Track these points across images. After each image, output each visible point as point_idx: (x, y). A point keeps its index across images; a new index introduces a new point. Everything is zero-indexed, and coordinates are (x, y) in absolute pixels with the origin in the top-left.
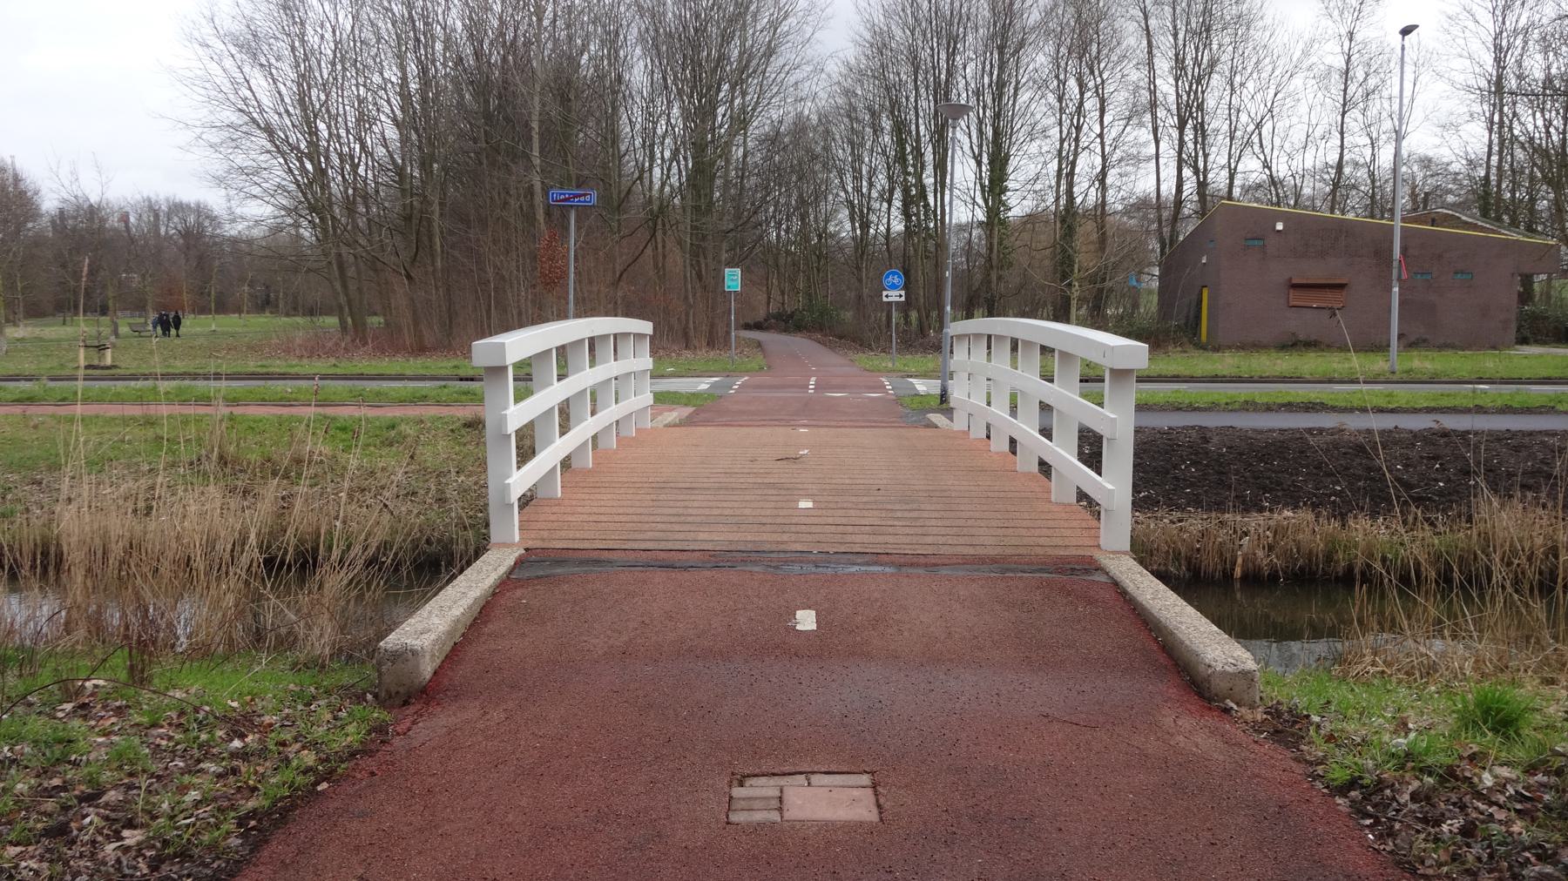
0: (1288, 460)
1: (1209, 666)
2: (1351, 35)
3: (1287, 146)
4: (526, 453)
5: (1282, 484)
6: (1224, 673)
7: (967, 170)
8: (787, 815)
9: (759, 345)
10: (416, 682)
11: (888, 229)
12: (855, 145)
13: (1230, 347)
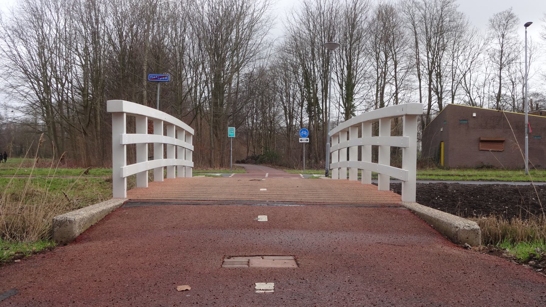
0: (484, 196)
1: (457, 227)
2: (503, 36)
3: (476, 84)
4: (132, 159)
5: (481, 205)
6: (464, 230)
7: (336, 91)
8: (251, 266)
9: (243, 167)
10: (71, 236)
11: (301, 122)
12: (287, 80)
13: (454, 168)
